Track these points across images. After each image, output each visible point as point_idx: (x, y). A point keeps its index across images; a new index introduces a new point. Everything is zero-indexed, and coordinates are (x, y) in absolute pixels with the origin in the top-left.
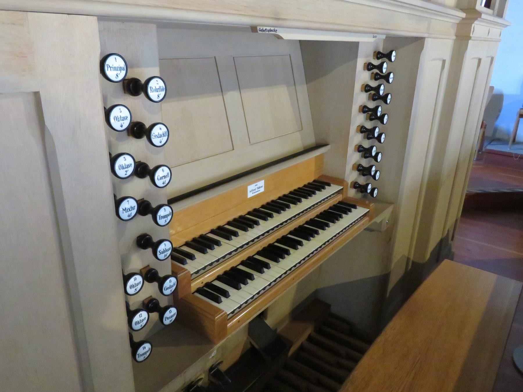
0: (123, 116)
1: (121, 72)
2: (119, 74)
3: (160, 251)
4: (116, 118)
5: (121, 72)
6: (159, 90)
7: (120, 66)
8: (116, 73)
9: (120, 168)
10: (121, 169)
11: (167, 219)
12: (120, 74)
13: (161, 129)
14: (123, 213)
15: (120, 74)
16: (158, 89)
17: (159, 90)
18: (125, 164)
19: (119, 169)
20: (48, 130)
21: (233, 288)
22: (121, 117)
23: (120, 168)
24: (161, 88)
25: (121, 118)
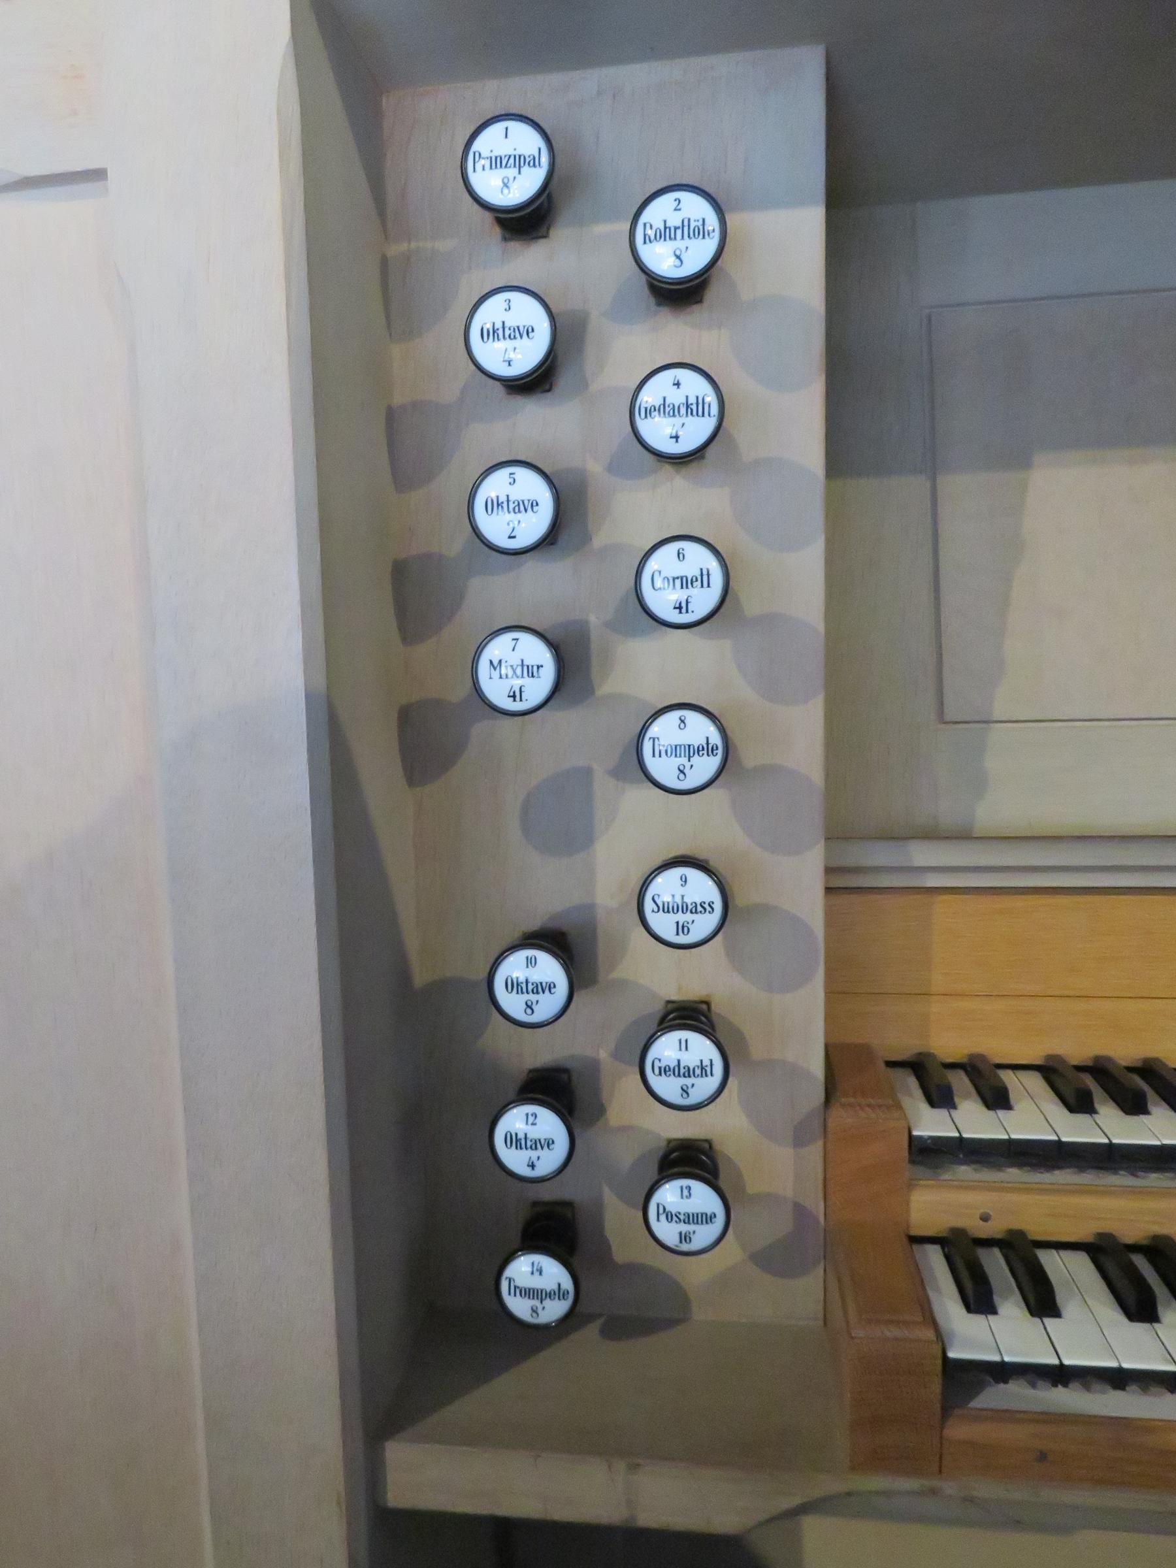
0: (520, 498)
1: (520, 173)
2: (511, 179)
3: (656, 898)
4: (531, 963)
5: (520, 173)
6: (679, 232)
7: (517, 153)
8: (531, 1305)
9: (533, 959)
10: (531, 958)
11: (688, 765)
12: (515, 178)
13: (678, 384)
14: (491, 678)
15: (515, 178)
16: (676, 228)
17: (679, 232)
18: (503, 323)
19: (535, 958)
20: (729, 1159)
21: (1121, 1311)
22: (508, 501)
23: (533, 959)
24: (693, 225)
25: (511, 503)
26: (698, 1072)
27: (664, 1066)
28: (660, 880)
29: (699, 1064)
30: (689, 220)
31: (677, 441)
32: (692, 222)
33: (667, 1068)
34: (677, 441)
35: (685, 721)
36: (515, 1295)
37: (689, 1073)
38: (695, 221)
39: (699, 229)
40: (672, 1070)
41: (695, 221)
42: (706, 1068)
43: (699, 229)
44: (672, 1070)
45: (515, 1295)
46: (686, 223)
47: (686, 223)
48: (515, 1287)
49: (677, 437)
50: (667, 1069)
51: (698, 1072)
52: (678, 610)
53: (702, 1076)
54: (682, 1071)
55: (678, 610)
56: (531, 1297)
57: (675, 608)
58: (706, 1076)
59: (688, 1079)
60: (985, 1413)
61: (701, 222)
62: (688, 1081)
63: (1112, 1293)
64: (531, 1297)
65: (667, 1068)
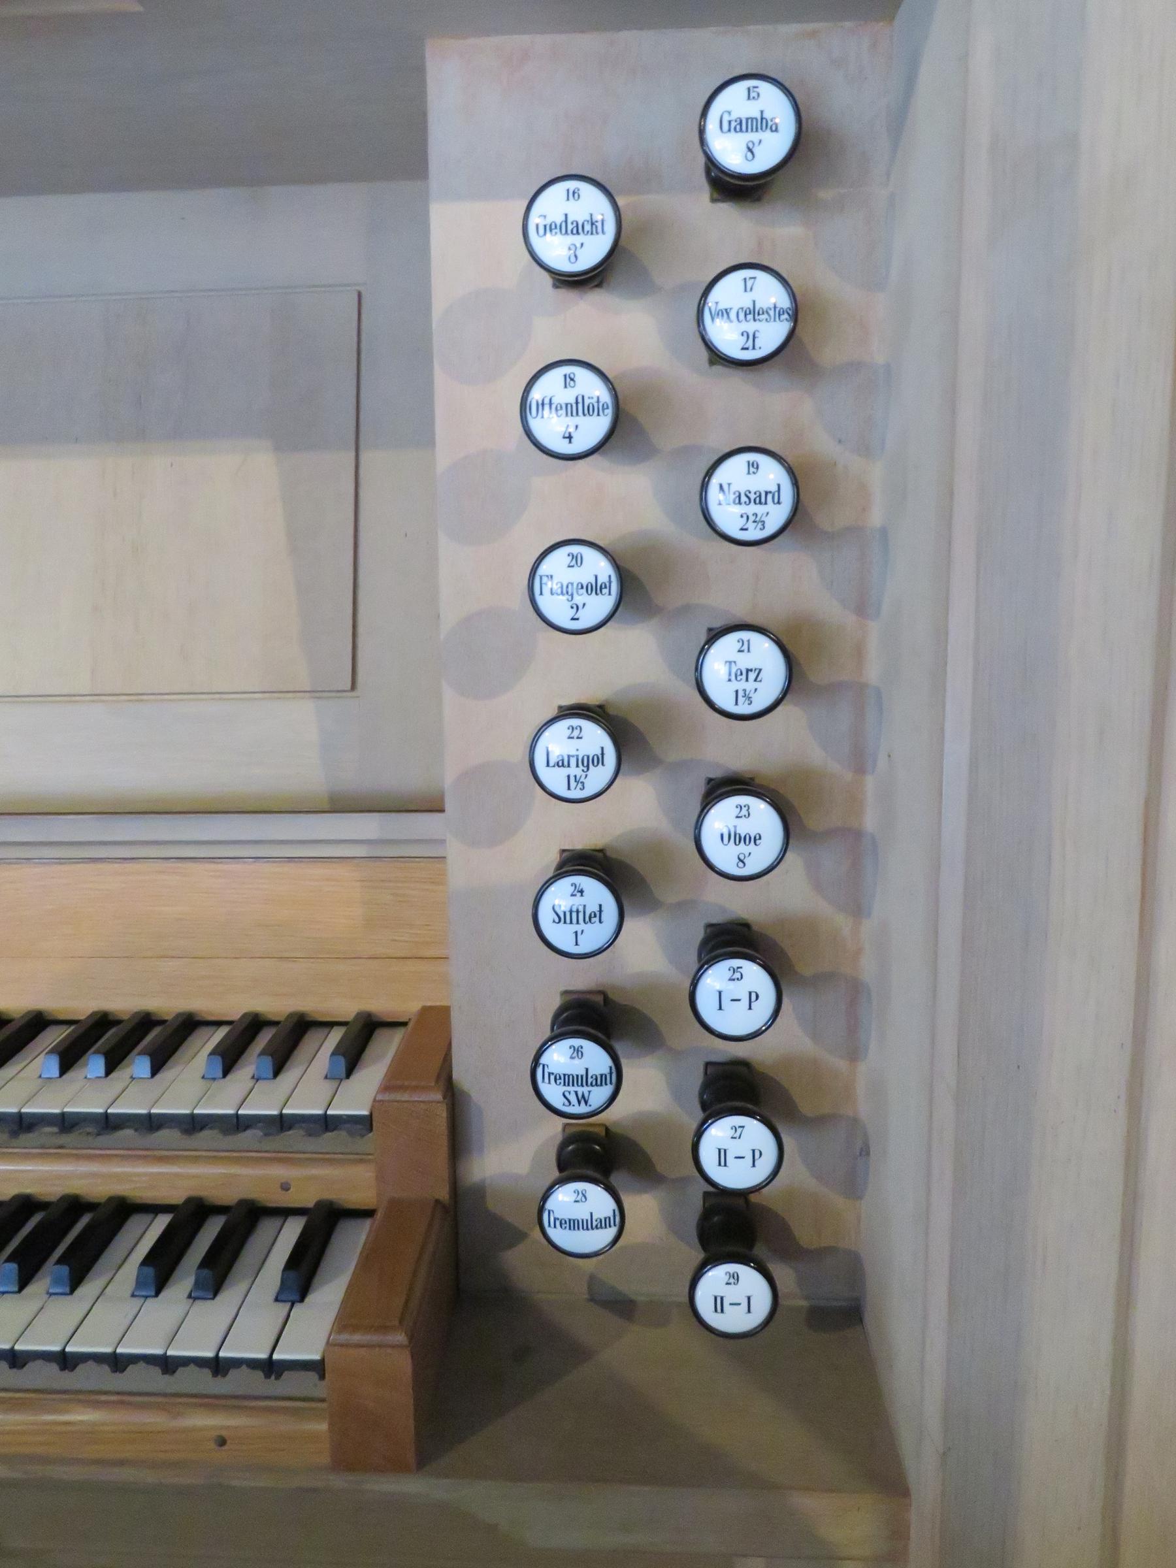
24: (587, 402)
26: (588, 227)
27: (549, 223)
28: (547, 734)
29: (589, 218)
30: (583, 397)
31: (570, 442)
32: (586, 399)
33: (553, 224)
34: (570, 442)
35: (575, 379)
36: (549, 1083)
37: (578, 229)
38: (589, 398)
39: (593, 406)
40: (558, 227)
41: (589, 398)
42: (596, 224)
43: (593, 406)
44: (558, 227)
45: (549, 1083)
46: (580, 400)
47: (580, 400)
48: (549, 1074)
49: (570, 437)
50: (553, 227)
51: (588, 227)
52: (568, 440)
53: (592, 234)
54: (570, 227)
55: (568, 440)
56: (572, 1228)
57: (564, 437)
58: (597, 233)
59: (576, 237)
60: (721, 958)
61: (595, 399)
62: (577, 240)
63: (19, 1052)
64: (572, 1228)
65: (553, 224)
